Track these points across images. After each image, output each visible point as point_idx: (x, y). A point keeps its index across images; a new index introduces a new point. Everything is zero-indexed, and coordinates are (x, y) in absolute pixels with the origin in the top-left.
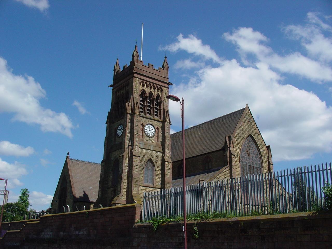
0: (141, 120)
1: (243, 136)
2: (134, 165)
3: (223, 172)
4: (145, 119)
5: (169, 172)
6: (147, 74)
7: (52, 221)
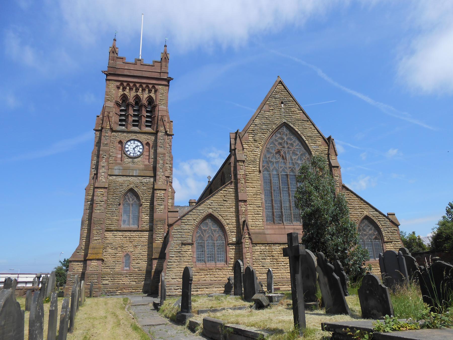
0: (118, 136)
1: (268, 127)
2: (97, 200)
3: (221, 192)
4: (125, 134)
5: (161, 204)
7: (209, 276)
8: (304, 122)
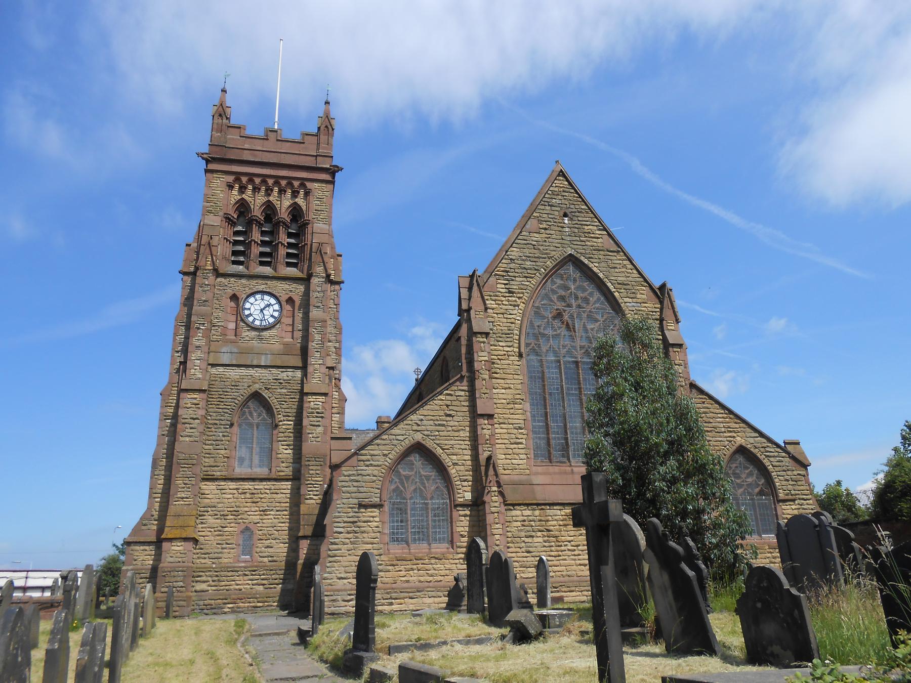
0: (229, 285)
2: (184, 416)
3: (441, 397)
6: (255, 156)
8: (610, 254)
